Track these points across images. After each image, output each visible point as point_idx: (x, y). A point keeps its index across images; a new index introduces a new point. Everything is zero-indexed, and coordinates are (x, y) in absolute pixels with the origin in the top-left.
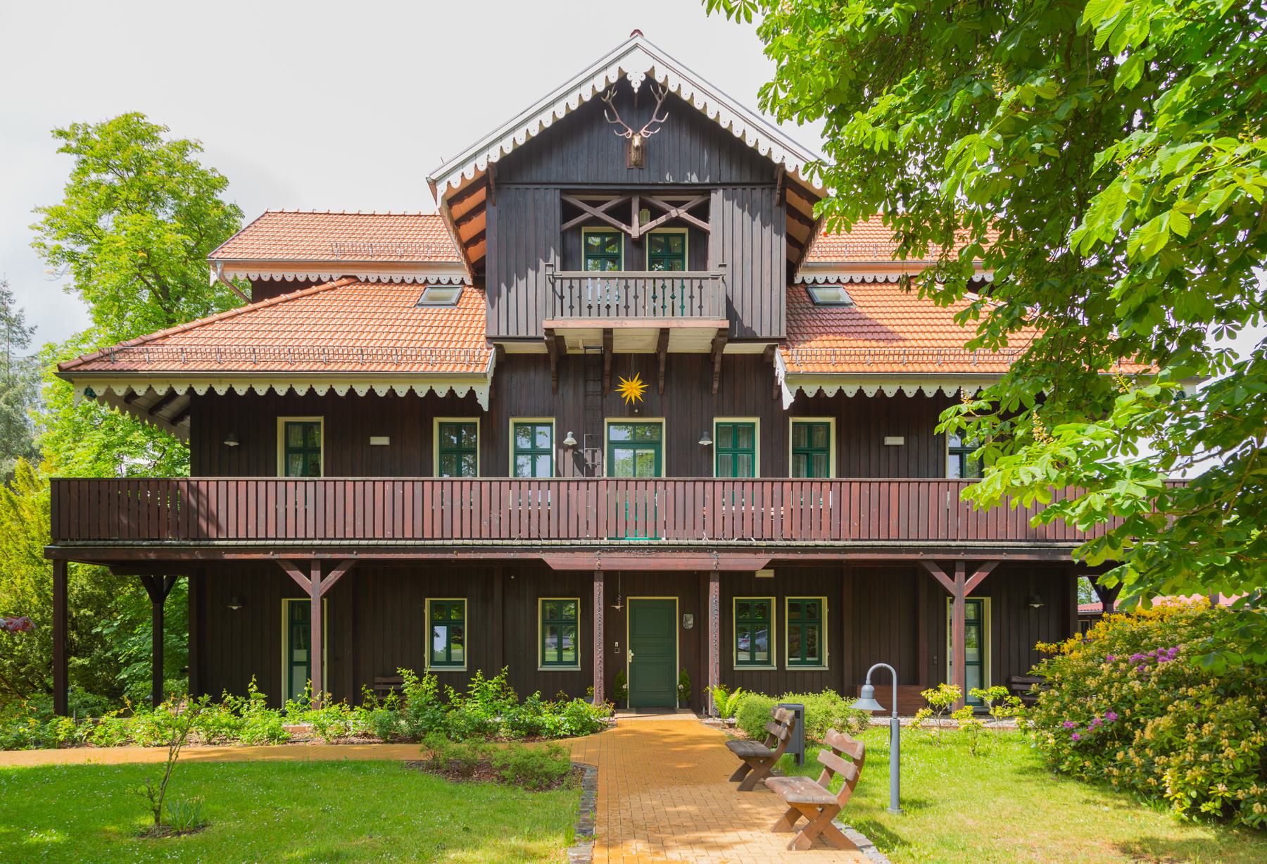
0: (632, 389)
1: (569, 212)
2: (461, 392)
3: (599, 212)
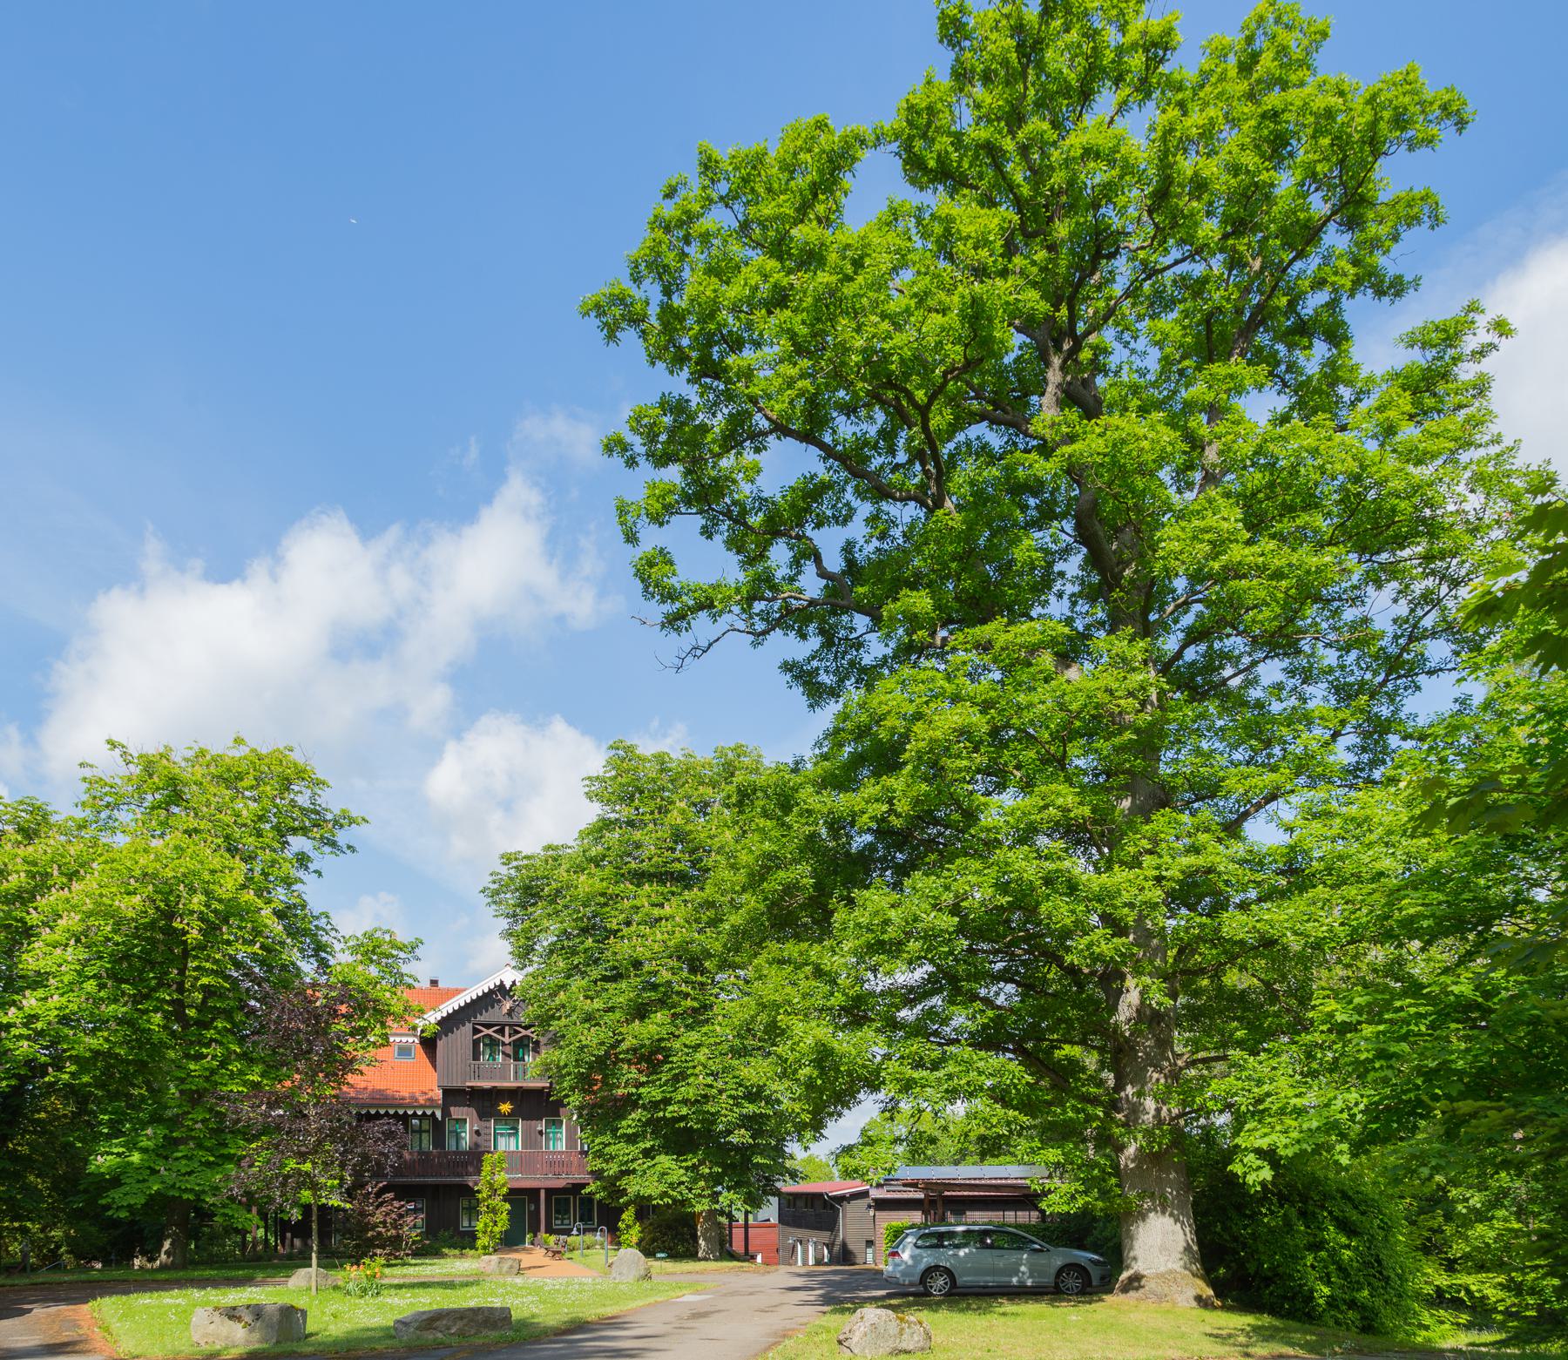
0: (505, 1108)
1: (476, 1031)
2: (429, 1112)
3: (490, 1032)
